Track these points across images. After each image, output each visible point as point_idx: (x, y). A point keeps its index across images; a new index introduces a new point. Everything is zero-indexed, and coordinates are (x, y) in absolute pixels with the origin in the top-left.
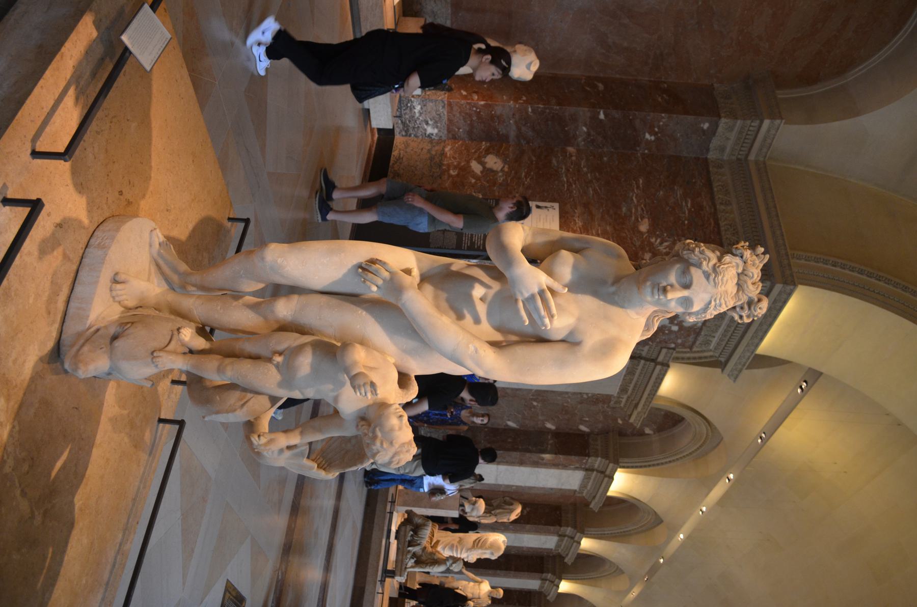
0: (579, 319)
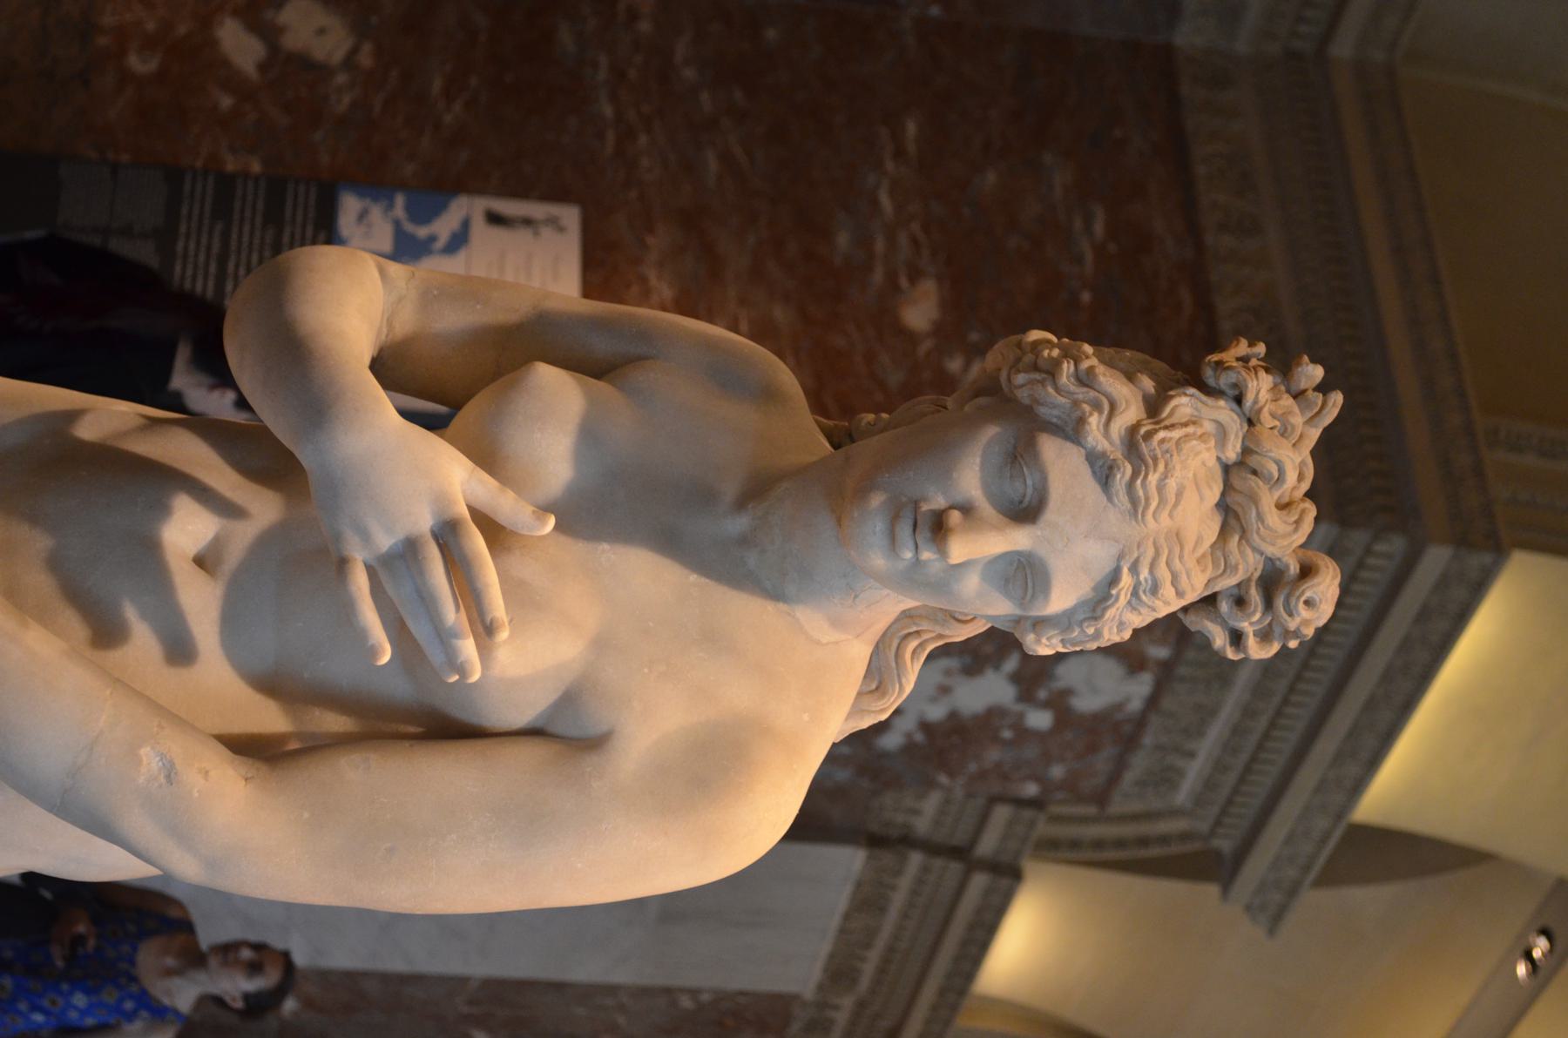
0: (601, 644)
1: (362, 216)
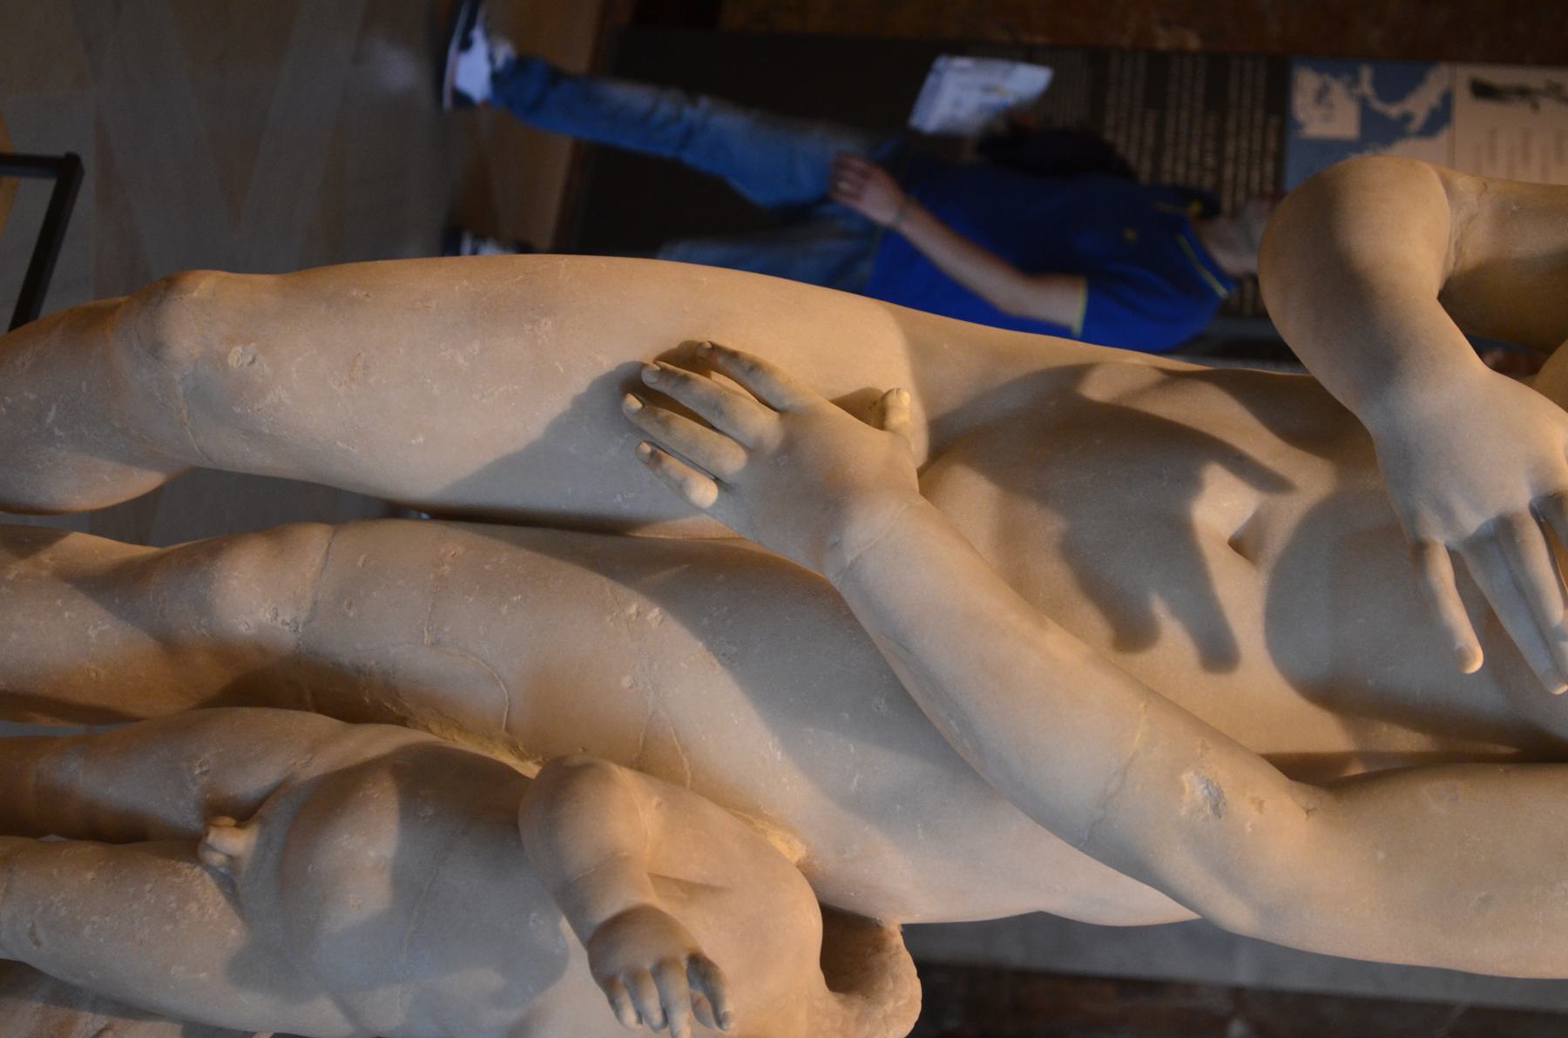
1: (1321, 96)
